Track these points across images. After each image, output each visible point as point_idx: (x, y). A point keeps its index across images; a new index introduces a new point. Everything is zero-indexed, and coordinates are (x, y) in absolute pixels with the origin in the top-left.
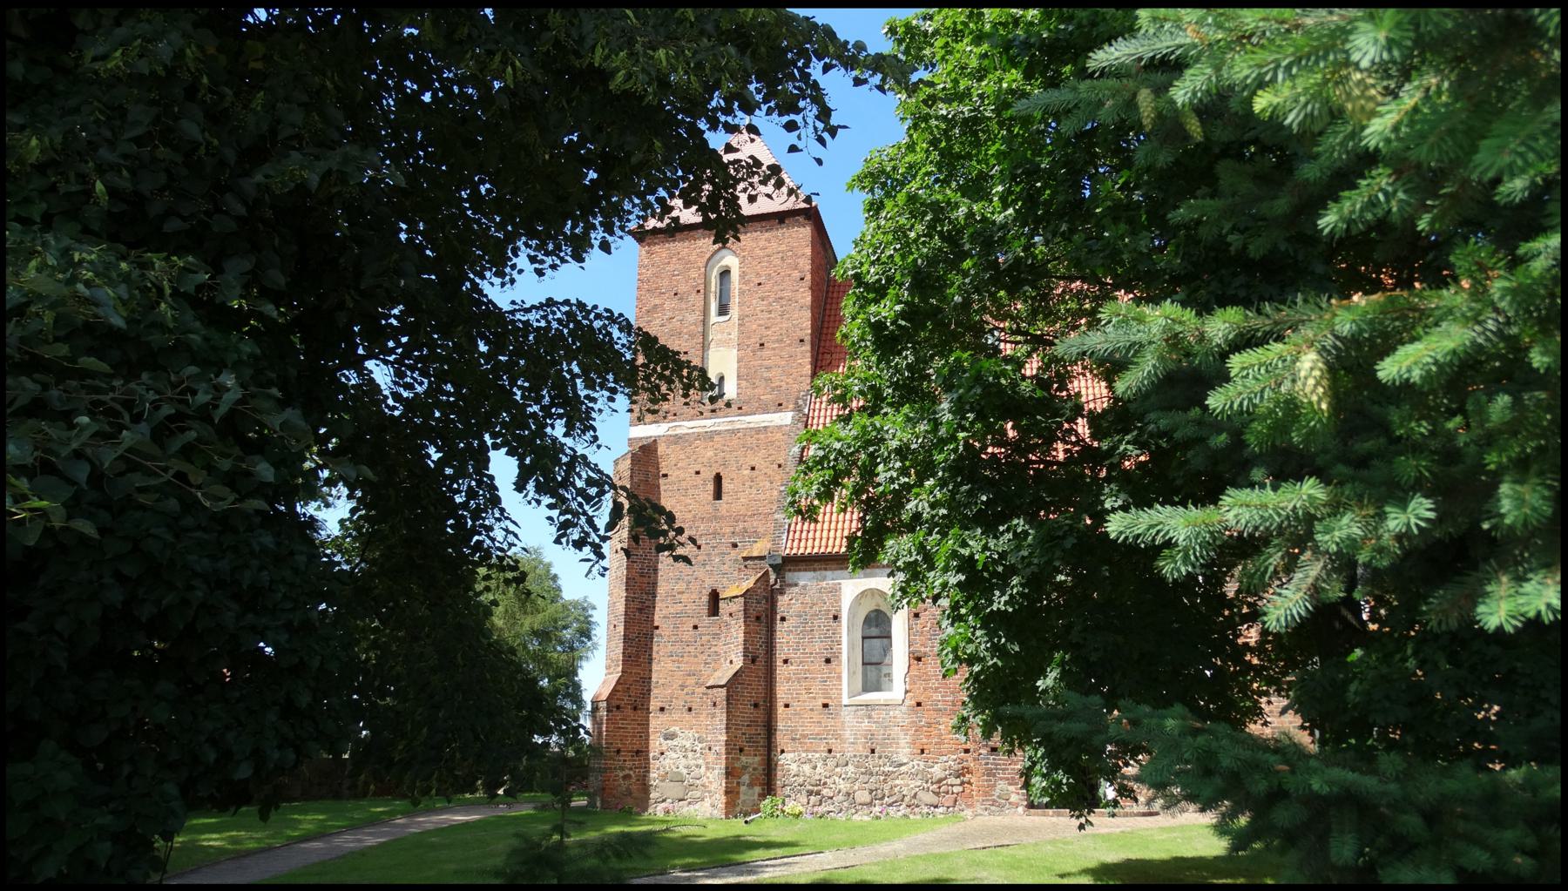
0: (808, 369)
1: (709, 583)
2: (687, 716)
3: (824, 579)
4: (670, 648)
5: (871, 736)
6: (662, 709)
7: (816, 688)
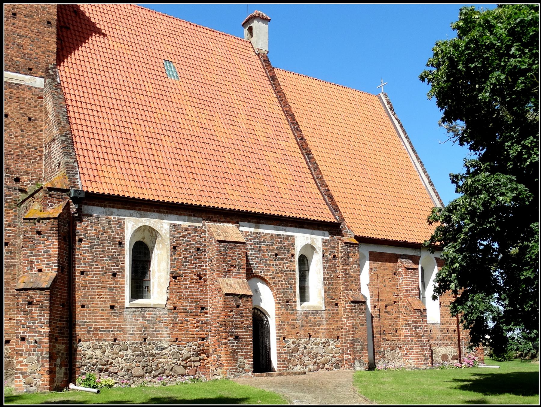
0: (54, 47)
5: (144, 329)
7: (106, 294)
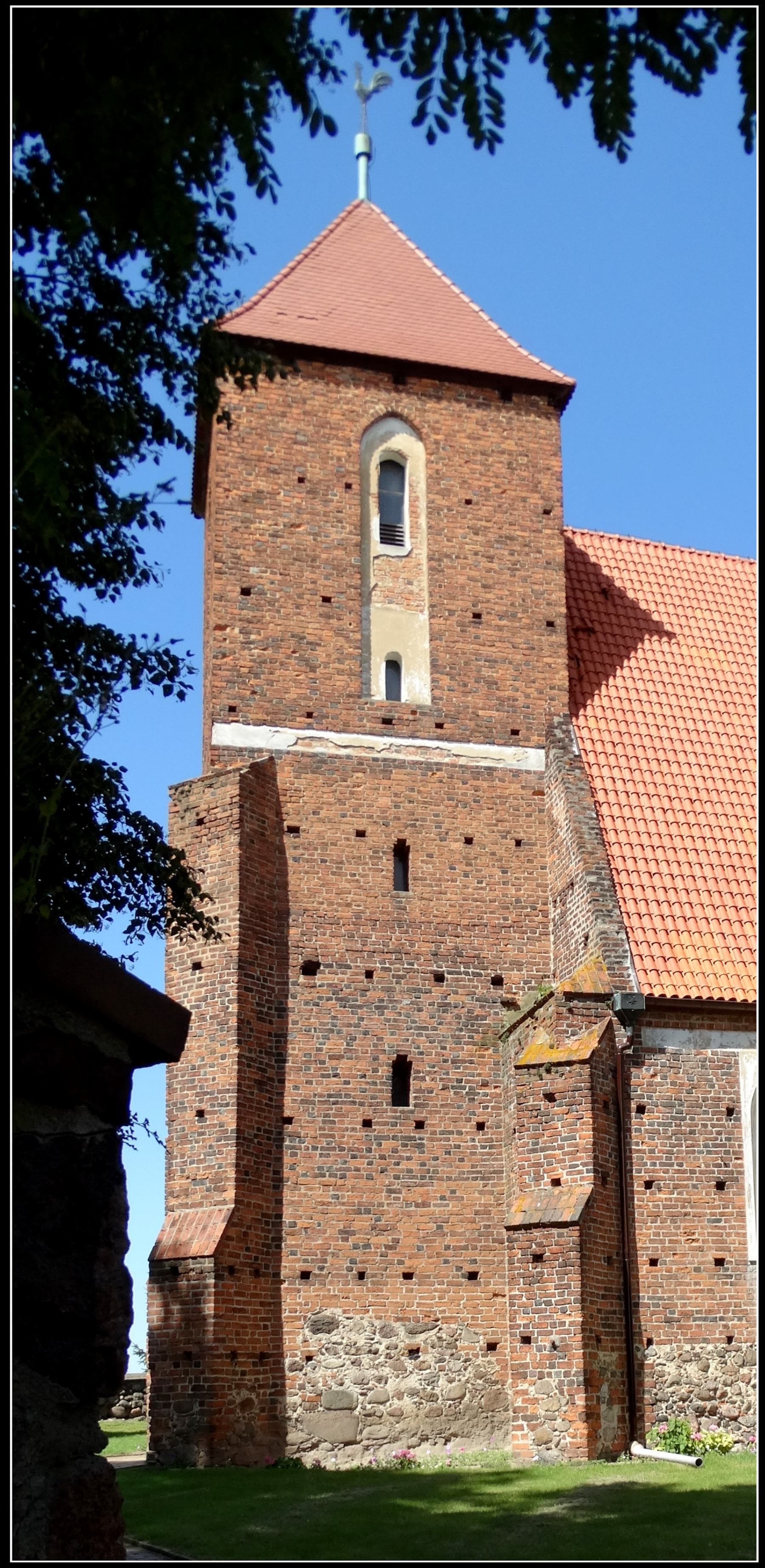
0: (562, 677)
1: (393, 1043)
2: (356, 1288)
3: (707, 1044)
4: (318, 1160)
6: (305, 1275)
7: (703, 1231)
